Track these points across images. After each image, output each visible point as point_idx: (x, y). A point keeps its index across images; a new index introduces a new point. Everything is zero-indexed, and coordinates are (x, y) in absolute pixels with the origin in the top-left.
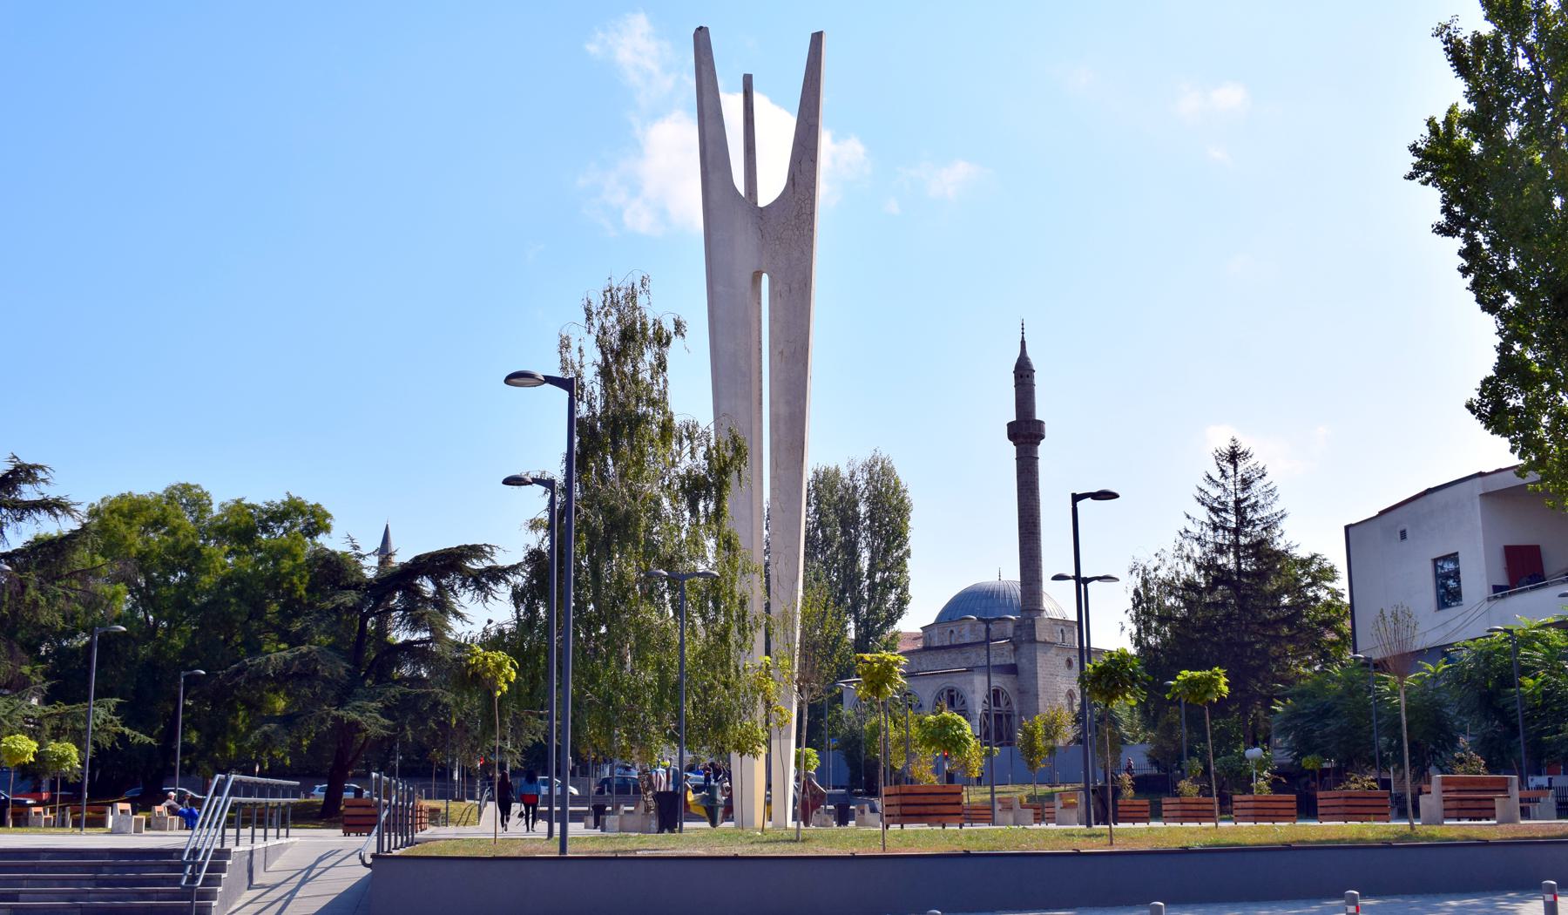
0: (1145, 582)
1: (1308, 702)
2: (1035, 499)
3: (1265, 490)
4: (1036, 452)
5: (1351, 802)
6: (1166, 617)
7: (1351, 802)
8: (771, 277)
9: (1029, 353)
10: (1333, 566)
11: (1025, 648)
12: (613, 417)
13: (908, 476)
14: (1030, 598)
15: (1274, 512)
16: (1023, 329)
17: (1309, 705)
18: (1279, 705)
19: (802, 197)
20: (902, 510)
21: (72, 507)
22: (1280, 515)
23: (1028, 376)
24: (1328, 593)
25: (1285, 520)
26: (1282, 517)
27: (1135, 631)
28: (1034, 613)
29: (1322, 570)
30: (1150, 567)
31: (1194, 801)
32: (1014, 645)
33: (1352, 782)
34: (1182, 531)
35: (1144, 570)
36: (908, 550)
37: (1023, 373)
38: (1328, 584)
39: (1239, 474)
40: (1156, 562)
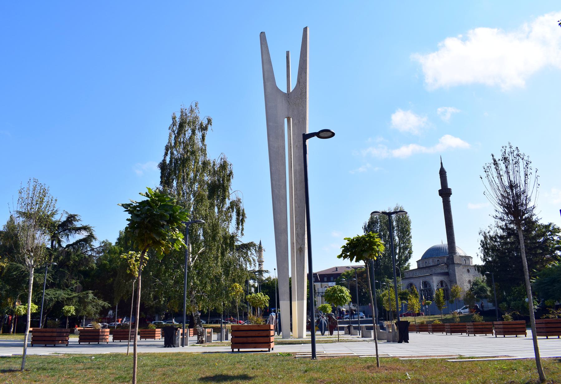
0: (485, 237)
1: (546, 278)
4: (449, 199)
5: (549, 325)
6: (493, 249)
7: (549, 325)
8: (292, 118)
9: (444, 166)
10: (559, 228)
11: (451, 266)
12: (509, 235)
15: (530, 206)
17: (547, 279)
18: (534, 280)
19: (302, 87)
20: (408, 223)
21: (91, 228)
22: (533, 208)
24: (558, 238)
25: (535, 209)
26: (534, 208)
27: (482, 256)
29: (554, 229)
30: (487, 232)
31: (480, 324)
33: (551, 314)
34: (495, 217)
35: (485, 233)
36: (411, 236)
37: (443, 173)
38: (557, 234)
40: (488, 229)
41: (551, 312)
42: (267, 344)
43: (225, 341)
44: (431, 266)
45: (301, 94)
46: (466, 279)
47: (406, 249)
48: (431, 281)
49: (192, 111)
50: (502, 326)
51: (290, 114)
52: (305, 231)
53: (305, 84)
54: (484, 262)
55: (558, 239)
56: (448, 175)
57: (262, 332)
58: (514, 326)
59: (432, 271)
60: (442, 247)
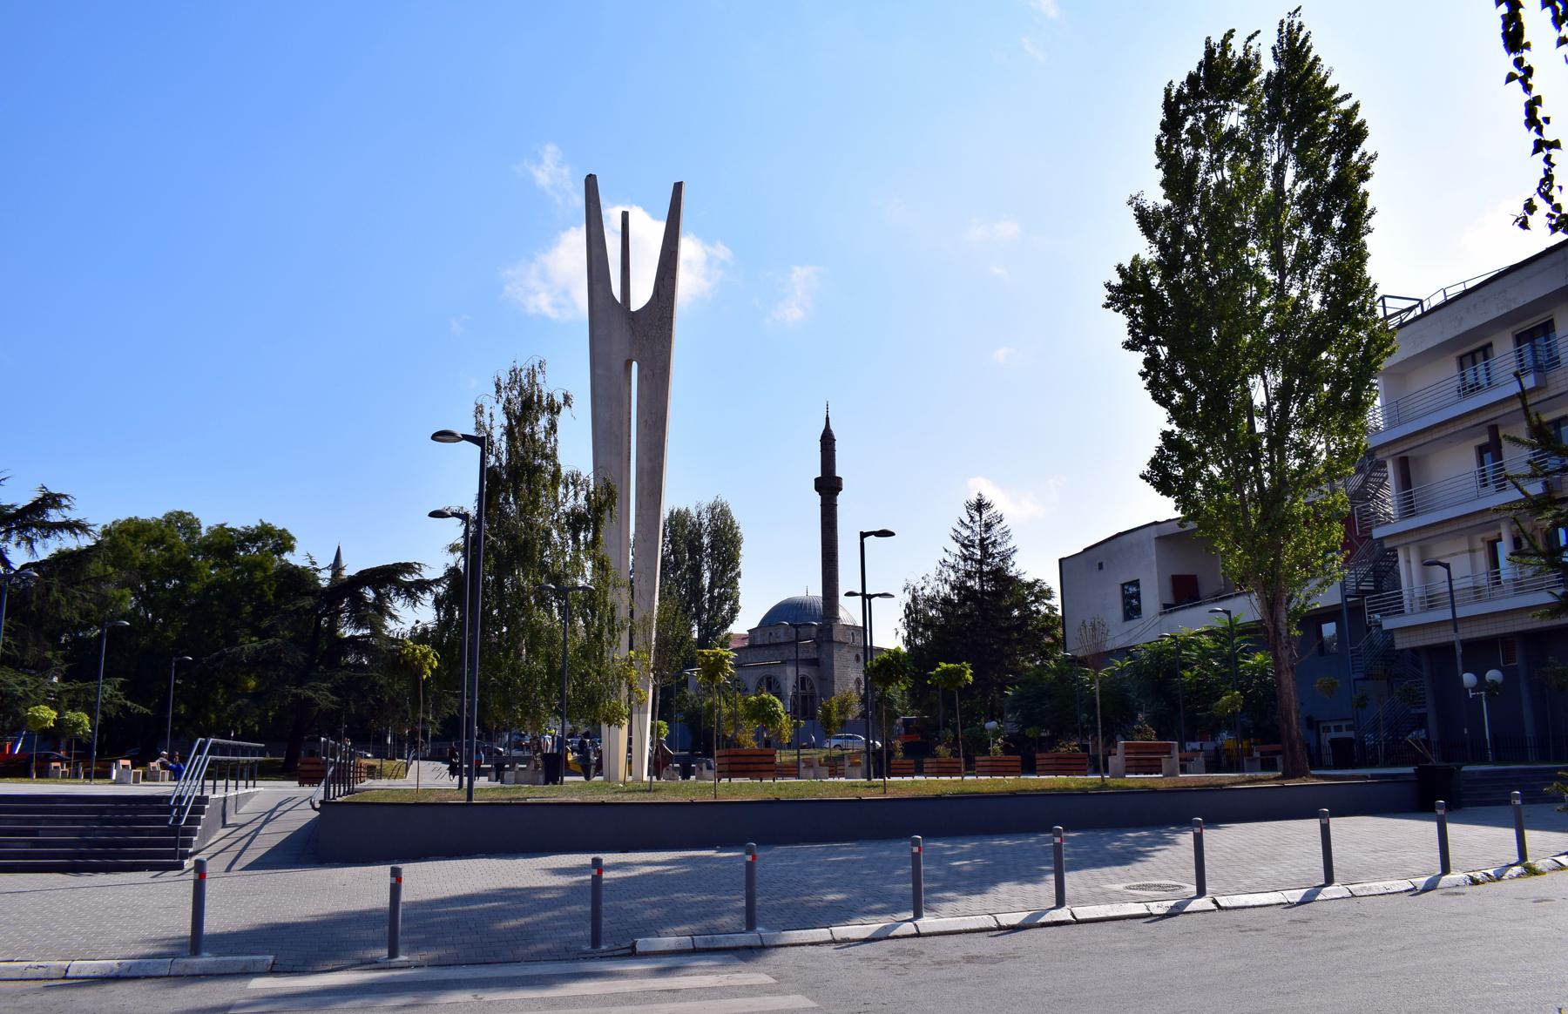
0: (914, 599)
3: (1002, 531)
4: (836, 501)
5: (1060, 761)
6: (929, 624)
7: (1060, 761)
8: (639, 364)
9: (832, 428)
13: (739, 516)
15: (1007, 548)
19: (664, 306)
22: (1012, 550)
25: (1016, 554)
29: (1042, 591)
32: (817, 644)
35: (914, 589)
37: (827, 441)
38: (1046, 601)
39: (984, 519)
40: (923, 584)
41: (1061, 744)
44: (781, 643)
47: (726, 598)
49: (532, 374)
55: (1047, 611)
58: (1006, 764)
59: (782, 654)
60: (808, 602)
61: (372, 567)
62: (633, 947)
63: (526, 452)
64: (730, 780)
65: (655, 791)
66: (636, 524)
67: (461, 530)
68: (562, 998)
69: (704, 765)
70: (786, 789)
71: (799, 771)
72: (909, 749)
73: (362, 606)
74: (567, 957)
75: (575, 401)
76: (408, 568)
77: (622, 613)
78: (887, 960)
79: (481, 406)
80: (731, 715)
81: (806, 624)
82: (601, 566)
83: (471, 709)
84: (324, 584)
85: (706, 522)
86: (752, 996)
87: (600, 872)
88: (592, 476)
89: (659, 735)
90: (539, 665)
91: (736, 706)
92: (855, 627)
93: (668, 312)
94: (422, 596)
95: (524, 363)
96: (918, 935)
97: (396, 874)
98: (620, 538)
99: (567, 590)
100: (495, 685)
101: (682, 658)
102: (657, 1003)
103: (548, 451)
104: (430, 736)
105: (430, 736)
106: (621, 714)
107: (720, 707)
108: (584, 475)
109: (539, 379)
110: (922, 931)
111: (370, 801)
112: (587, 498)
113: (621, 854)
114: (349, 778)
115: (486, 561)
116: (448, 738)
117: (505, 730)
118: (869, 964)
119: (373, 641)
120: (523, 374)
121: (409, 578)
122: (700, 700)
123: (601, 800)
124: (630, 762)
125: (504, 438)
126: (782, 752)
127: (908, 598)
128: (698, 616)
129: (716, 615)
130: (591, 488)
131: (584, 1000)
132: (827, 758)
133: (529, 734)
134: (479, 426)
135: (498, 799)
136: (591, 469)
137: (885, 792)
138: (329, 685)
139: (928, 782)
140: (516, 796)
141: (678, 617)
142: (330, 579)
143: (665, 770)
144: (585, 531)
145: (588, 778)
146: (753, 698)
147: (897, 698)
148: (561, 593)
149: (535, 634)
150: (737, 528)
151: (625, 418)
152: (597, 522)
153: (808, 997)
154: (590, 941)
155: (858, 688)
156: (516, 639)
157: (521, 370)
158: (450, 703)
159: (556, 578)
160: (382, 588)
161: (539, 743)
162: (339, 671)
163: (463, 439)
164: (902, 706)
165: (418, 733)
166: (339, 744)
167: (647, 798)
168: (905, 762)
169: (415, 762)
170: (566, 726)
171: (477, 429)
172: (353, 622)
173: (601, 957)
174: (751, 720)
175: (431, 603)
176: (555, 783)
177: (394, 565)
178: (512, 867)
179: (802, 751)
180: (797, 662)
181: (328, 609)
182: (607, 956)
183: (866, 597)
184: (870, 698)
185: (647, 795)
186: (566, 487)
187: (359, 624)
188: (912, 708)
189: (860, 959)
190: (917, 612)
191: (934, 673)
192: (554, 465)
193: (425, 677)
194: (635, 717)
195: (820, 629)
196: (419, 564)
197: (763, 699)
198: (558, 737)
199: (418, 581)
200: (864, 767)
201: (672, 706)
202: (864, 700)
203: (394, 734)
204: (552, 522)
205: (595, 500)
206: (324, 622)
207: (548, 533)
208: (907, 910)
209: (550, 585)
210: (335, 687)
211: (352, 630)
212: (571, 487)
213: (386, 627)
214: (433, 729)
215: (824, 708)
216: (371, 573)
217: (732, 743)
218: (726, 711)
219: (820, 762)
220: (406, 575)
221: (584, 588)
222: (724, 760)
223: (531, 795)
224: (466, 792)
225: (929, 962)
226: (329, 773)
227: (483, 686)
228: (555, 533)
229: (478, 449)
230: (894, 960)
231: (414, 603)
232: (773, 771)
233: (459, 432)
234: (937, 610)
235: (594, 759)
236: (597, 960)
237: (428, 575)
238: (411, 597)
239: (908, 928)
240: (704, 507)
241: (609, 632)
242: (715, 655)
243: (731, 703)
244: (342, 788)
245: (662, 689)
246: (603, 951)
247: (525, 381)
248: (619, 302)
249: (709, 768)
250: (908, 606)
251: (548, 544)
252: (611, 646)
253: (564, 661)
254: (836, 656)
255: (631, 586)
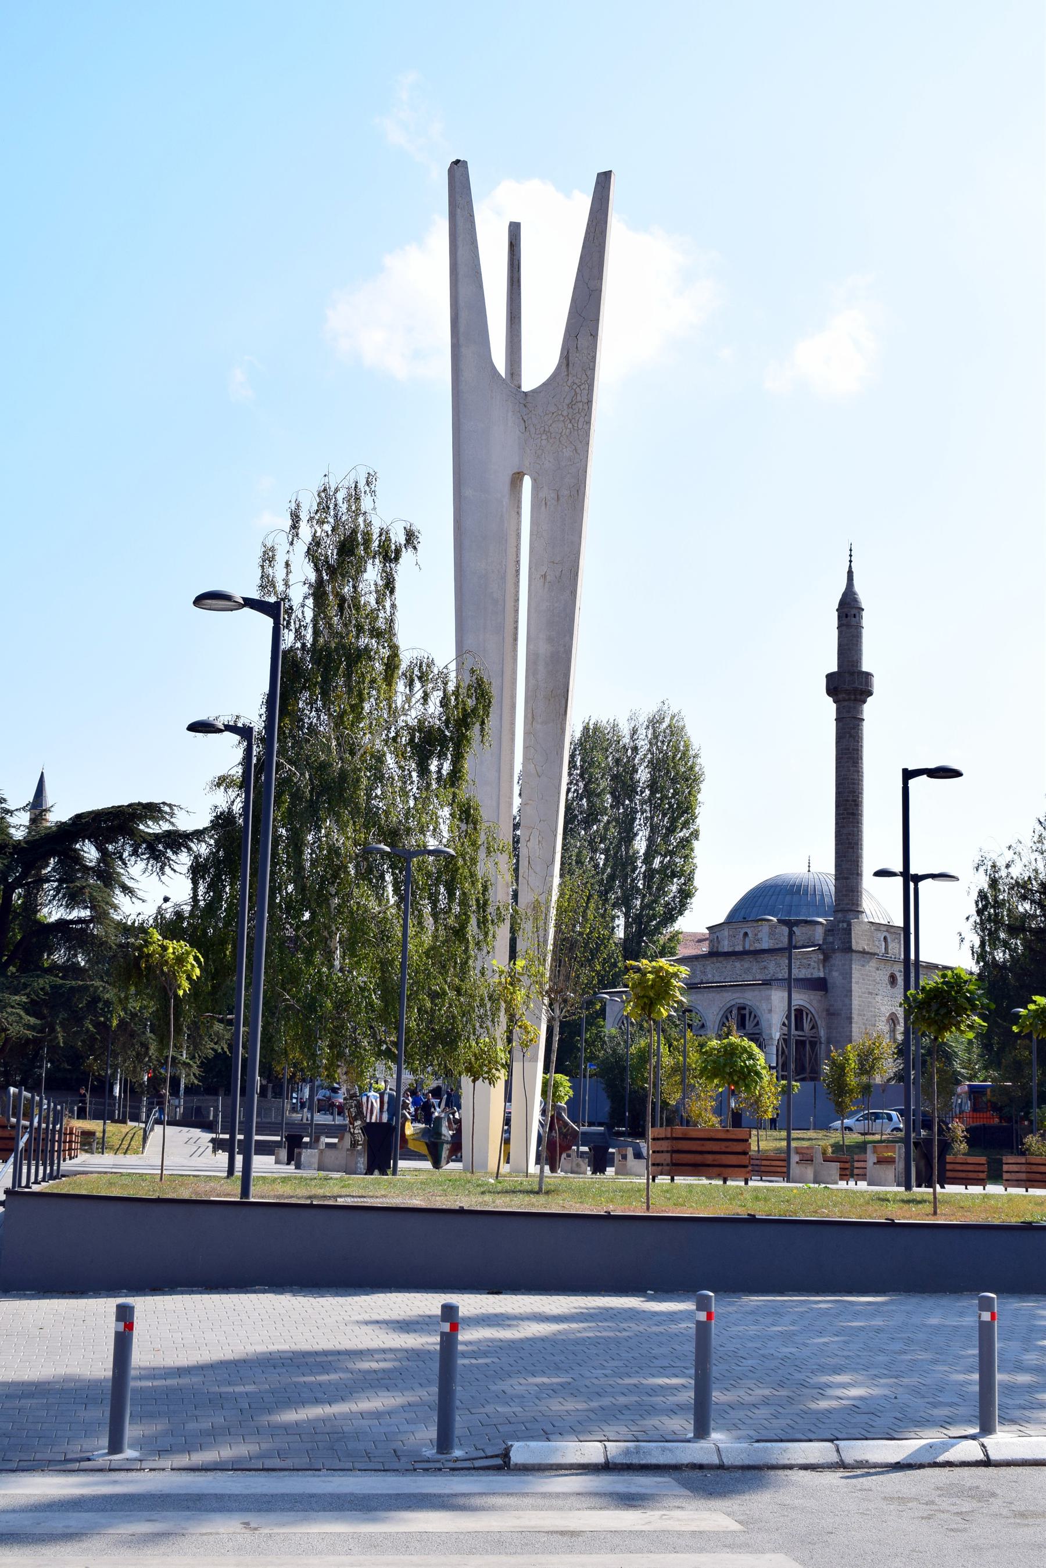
0: (994, 883)
2: (859, 772)
4: (861, 712)
8: (534, 481)
9: (858, 587)
11: (838, 959)
14: (846, 895)
16: (851, 556)
19: (577, 381)
23: (855, 616)
28: (851, 915)
30: (1001, 863)
32: (824, 953)
35: (994, 866)
40: (1009, 856)
42: (743, 1169)
43: (452, 1165)
45: (570, 406)
46: (883, 1009)
48: (764, 1006)
49: (355, 497)
50: (1024, 1168)
51: (527, 463)
52: (554, 853)
53: (589, 373)
54: (978, 962)
56: (868, 621)
57: (735, 1143)
61: (95, 808)
62: (506, 1455)
63: (345, 625)
64: (672, 1180)
65: (547, 1193)
66: (525, 733)
67: (239, 754)
68: (387, 1536)
69: (630, 1151)
70: (766, 1200)
71: (788, 1167)
72: (977, 1138)
73: (78, 870)
74: (396, 1466)
75: (424, 541)
76: (152, 810)
77: (500, 895)
78: (933, 1503)
79: (272, 549)
80: (675, 1070)
81: (806, 922)
82: (466, 814)
83: (249, 1046)
84: (18, 834)
85: (643, 744)
86: (701, 1550)
87: (454, 1327)
88: (453, 666)
89: (556, 1097)
90: (362, 977)
91: (685, 1055)
92: (889, 928)
93: (585, 392)
94: (174, 857)
95: (340, 479)
96: (987, 1463)
97: (125, 1315)
98: (499, 771)
99: (409, 855)
100: (290, 1007)
101: (598, 973)
102: (543, 1553)
103: (381, 624)
104: (182, 1086)
105: (182, 1086)
106: (493, 1062)
107: (658, 1054)
108: (439, 664)
109: (366, 503)
110: (994, 1456)
111: (84, 1192)
112: (444, 703)
113: (490, 1296)
114: (52, 1151)
115: (278, 802)
116: (211, 1090)
117: (304, 1080)
118: (900, 1508)
119: (96, 930)
120: (341, 495)
121: (152, 828)
122: (626, 1042)
123: (456, 1206)
124: (507, 1141)
125: (310, 602)
126: (762, 1133)
127: (983, 883)
128: (625, 902)
129: (655, 901)
130: (451, 687)
131: (425, 1541)
132: (837, 1147)
133: (343, 1090)
134: (267, 583)
135: (292, 1197)
136: (452, 654)
137: (935, 1213)
138: (24, 999)
139: (1010, 1199)
140: (321, 1192)
141: (592, 905)
142: (28, 828)
143: (564, 1155)
144: (439, 757)
145: (437, 1164)
146: (714, 1043)
147: (960, 1050)
148: (401, 859)
149: (358, 925)
150: (696, 756)
151: (511, 571)
152: (460, 742)
153: (796, 1560)
154: (435, 1443)
155: (893, 1031)
156: (326, 934)
157: (337, 490)
158: (217, 1034)
159: (392, 835)
160: (111, 843)
161: (359, 1105)
162: (38, 976)
163: (244, 606)
164: (968, 1064)
165: (165, 1082)
166: (37, 1098)
167: (533, 1205)
168: (971, 1159)
169: (158, 1128)
170: (403, 1076)
171: (262, 587)
172: (64, 897)
173: (453, 1469)
174: (710, 1078)
175: (184, 869)
176: (383, 1173)
177: (130, 805)
178: (310, 1311)
179: (795, 1134)
180: (790, 983)
181: (25, 874)
182: (462, 1469)
183: (910, 879)
184: (913, 1048)
185: (533, 1199)
186: (411, 684)
187: (73, 899)
188: (985, 1068)
189: (885, 1498)
190: (998, 904)
191: (1023, 1011)
192: (390, 647)
193: (181, 993)
194: (517, 1067)
195: (830, 930)
196: (170, 806)
197: (731, 1044)
198: (390, 1095)
199: (168, 834)
200: (901, 1165)
201: (579, 1050)
202: (902, 1051)
203: (126, 1080)
204: (386, 742)
205: (456, 707)
206: (17, 897)
207: (380, 759)
208: (969, 1422)
209: (382, 846)
210: (32, 1001)
211: (62, 910)
212: (417, 685)
213: (116, 907)
214: (188, 1075)
215: (834, 1063)
216: (93, 819)
217: (673, 1116)
218: (667, 1061)
219: (824, 1153)
220: (150, 823)
221: (436, 853)
222: (664, 1145)
223: (344, 1191)
224: (239, 1183)
225: (1005, 1512)
226: (22, 1144)
227: (270, 1009)
228: (390, 760)
229: (269, 622)
230: (944, 1503)
231: (162, 869)
232: (745, 1166)
233: (239, 593)
234: (1033, 902)
235: (447, 1133)
236: (445, 1475)
237: (185, 823)
238: (156, 858)
239: (970, 1450)
240: (643, 719)
241: (479, 927)
242: (657, 971)
243: (677, 1049)
244: (41, 1168)
245: (563, 1025)
246: (457, 1460)
247: (343, 508)
248: (504, 376)
249: (638, 1155)
250: (982, 895)
251: (379, 777)
252: (479, 949)
253: (403, 972)
254: (856, 975)
255: (515, 849)
